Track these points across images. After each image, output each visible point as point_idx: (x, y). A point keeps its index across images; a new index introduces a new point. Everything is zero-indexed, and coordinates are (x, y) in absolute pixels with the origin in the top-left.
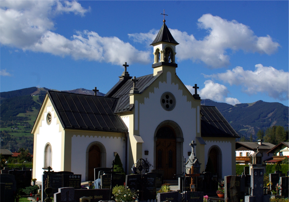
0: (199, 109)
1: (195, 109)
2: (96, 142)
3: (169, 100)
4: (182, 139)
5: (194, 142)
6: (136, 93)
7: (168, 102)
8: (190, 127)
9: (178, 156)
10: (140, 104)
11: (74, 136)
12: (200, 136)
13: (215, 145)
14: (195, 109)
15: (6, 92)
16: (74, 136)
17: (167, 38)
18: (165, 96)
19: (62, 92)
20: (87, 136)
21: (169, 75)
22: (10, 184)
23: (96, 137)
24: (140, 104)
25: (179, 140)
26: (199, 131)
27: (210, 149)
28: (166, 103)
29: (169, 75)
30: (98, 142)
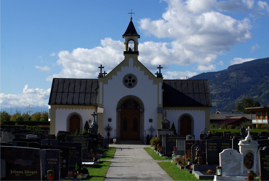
0: (161, 85)
1: (157, 85)
2: (75, 113)
3: (131, 80)
4: (143, 109)
5: (243, 127)
6: (101, 77)
7: (130, 81)
8: (151, 100)
9: (141, 122)
10: (104, 85)
11: (58, 109)
12: (162, 106)
13: (186, 114)
14: (157, 85)
15: (221, 71)
16: (58, 109)
17: (131, 33)
18: (128, 77)
19: (266, 58)
20: (68, 109)
21: (131, 60)
22: (20, 172)
23: (74, 109)
24: (104, 85)
25: (141, 110)
26: (161, 102)
27: (180, 116)
28: (128, 83)
29: (131, 60)
30: (76, 113)
